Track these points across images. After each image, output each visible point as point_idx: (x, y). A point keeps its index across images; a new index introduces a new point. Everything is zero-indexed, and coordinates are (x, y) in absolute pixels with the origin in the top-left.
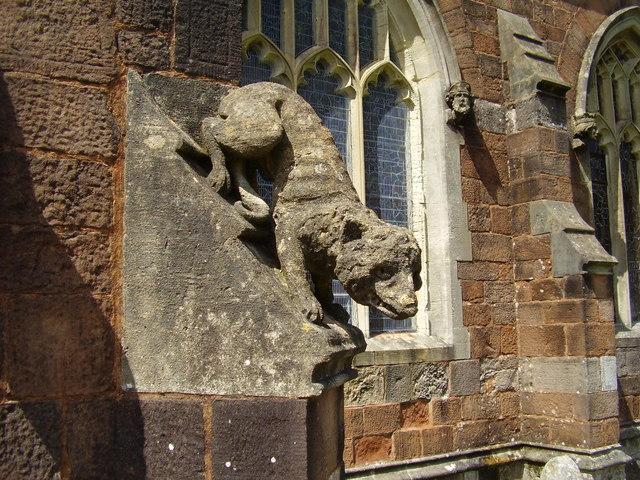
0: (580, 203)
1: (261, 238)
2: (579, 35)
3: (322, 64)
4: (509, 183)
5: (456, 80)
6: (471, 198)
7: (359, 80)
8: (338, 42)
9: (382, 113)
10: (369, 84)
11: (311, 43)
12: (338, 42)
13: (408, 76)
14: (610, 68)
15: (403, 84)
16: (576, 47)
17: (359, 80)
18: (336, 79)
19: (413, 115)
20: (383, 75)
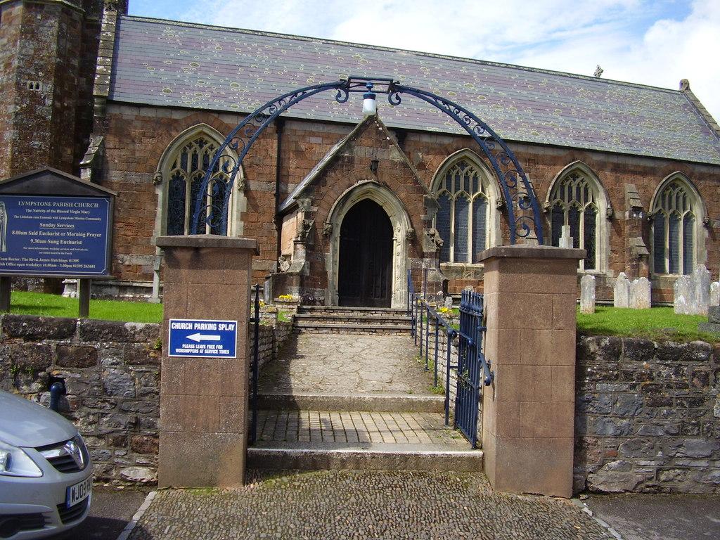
0: (646, 240)
1: (433, 241)
2: (550, 175)
3: (574, 205)
4: (260, 210)
5: (500, 196)
6: (503, 229)
7: (471, 198)
8: (467, 189)
9: (479, 206)
10: (475, 199)
11: (477, 191)
12: (467, 189)
13: (487, 196)
14: (668, 192)
15: (485, 198)
16: (548, 179)
17: (471, 198)
18: (466, 198)
19: (488, 206)
20: (590, 206)
